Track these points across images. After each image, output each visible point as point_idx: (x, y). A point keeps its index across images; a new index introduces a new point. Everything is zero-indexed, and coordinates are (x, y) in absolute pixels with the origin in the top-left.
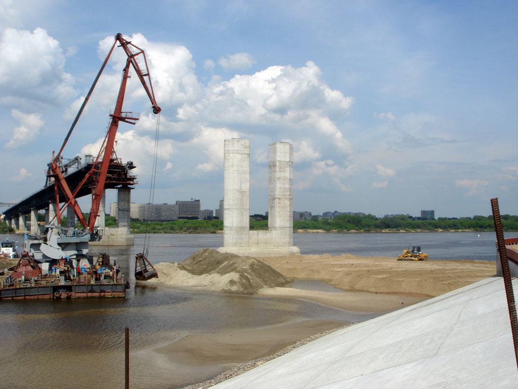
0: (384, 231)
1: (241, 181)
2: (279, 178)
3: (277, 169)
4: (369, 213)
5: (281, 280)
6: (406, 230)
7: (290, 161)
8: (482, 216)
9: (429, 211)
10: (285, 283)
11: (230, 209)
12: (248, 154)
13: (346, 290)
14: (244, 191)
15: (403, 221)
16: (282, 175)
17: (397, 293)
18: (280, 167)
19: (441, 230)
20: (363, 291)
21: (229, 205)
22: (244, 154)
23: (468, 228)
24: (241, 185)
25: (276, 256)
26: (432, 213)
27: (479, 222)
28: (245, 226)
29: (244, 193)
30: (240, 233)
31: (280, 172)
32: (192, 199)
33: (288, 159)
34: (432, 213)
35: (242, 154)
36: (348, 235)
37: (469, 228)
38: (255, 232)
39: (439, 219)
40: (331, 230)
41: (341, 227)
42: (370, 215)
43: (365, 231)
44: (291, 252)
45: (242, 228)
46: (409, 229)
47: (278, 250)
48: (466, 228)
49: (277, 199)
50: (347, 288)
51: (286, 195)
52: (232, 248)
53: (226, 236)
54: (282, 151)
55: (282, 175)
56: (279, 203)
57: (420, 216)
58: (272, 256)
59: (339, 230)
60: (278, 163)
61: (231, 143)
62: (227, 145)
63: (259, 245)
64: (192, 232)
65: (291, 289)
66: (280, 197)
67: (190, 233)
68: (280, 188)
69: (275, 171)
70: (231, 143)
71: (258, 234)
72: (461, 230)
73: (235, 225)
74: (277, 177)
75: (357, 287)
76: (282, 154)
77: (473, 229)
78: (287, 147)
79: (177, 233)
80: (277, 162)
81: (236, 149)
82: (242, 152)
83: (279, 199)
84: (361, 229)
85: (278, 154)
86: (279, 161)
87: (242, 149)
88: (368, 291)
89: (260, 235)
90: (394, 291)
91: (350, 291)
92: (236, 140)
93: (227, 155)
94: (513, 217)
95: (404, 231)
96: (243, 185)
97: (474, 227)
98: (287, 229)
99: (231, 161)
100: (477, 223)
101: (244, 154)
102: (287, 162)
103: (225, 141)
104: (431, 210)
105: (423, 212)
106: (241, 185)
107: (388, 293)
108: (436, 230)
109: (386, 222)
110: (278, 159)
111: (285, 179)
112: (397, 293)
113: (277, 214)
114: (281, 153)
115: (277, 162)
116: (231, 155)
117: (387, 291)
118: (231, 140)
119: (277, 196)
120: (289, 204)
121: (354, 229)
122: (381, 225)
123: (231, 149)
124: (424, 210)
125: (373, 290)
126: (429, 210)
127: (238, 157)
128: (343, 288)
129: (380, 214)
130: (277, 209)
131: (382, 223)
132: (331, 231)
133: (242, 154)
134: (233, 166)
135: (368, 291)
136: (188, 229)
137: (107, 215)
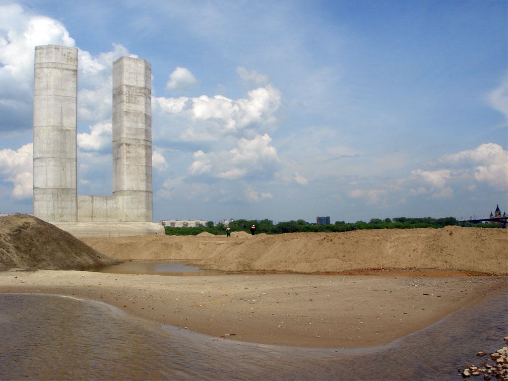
2: (127, 113)
3: (125, 98)
4: (266, 218)
5: (86, 259)
7: (145, 88)
8: (378, 220)
9: (324, 218)
10: (99, 266)
12: (74, 70)
13: (230, 273)
15: (300, 225)
16: (133, 107)
17: (375, 271)
18: (130, 96)
20: (274, 272)
22: (67, 69)
25: (122, 235)
26: (328, 219)
28: (69, 186)
29: (67, 133)
30: (59, 198)
33: (142, 84)
34: (328, 219)
35: (63, 69)
39: (337, 223)
42: (267, 220)
44: (148, 230)
49: (125, 146)
50: (233, 267)
51: (139, 140)
54: (132, 71)
55: (133, 107)
56: (128, 152)
57: (316, 223)
58: (116, 235)
60: (125, 89)
61: (45, 51)
66: (128, 142)
68: (129, 129)
69: (122, 102)
73: (51, 184)
74: (125, 110)
75: (258, 265)
76: (132, 76)
80: (125, 87)
81: (53, 61)
82: (64, 66)
83: (128, 145)
85: (126, 75)
86: (127, 86)
87: (63, 62)
88: (290, 272)
90: (363, 266)
91: (240, 273)
93: (38, 71)
94: (409, 219)
98: (142, 193)
101: (67, 69)
102: (141, 89)
103: (36, 49)
104: (326, 216)
105: (319, 219)
106: (62, 118)
107: (350, 273)
109: (283, 226)
110: (125, 82)
111: (137, 114)
112: (375, 271)
113: (124, 169)
114: (130, 73)
115: (125, 87)
116: (45, 70)
117: (346, 266)
119: (124, 141)
122: (278, 230)
123: (44, 60)
124: (320, 217)
125: (304, 267)
126: (324, 216)
127: (57, 73)
128: (224, 268)
130: (125, 162)
131: (279, 227)
134: (47, 88)
135: (290, 272)
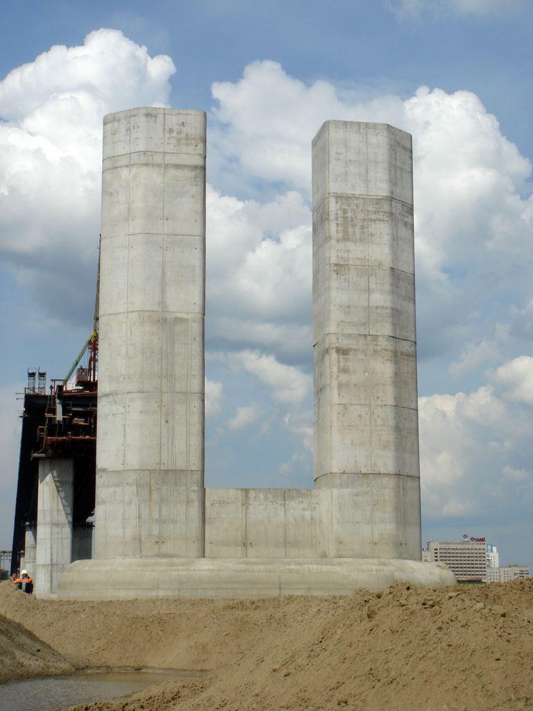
1: (163, 274)
22: (177, 166)
24: (163, 292)
28: (180, 464)
29: (179, 329)
30: (155, 496)
31: (346, 238)
32: (465, 536)
49: (334, 354)
51: (375, 337)
54: (352, 157)
68: (347, 308)
76: (352, 169)
80: (332, 201)
82: (170, 159)
101: (177, 166)
106: (163, 292)
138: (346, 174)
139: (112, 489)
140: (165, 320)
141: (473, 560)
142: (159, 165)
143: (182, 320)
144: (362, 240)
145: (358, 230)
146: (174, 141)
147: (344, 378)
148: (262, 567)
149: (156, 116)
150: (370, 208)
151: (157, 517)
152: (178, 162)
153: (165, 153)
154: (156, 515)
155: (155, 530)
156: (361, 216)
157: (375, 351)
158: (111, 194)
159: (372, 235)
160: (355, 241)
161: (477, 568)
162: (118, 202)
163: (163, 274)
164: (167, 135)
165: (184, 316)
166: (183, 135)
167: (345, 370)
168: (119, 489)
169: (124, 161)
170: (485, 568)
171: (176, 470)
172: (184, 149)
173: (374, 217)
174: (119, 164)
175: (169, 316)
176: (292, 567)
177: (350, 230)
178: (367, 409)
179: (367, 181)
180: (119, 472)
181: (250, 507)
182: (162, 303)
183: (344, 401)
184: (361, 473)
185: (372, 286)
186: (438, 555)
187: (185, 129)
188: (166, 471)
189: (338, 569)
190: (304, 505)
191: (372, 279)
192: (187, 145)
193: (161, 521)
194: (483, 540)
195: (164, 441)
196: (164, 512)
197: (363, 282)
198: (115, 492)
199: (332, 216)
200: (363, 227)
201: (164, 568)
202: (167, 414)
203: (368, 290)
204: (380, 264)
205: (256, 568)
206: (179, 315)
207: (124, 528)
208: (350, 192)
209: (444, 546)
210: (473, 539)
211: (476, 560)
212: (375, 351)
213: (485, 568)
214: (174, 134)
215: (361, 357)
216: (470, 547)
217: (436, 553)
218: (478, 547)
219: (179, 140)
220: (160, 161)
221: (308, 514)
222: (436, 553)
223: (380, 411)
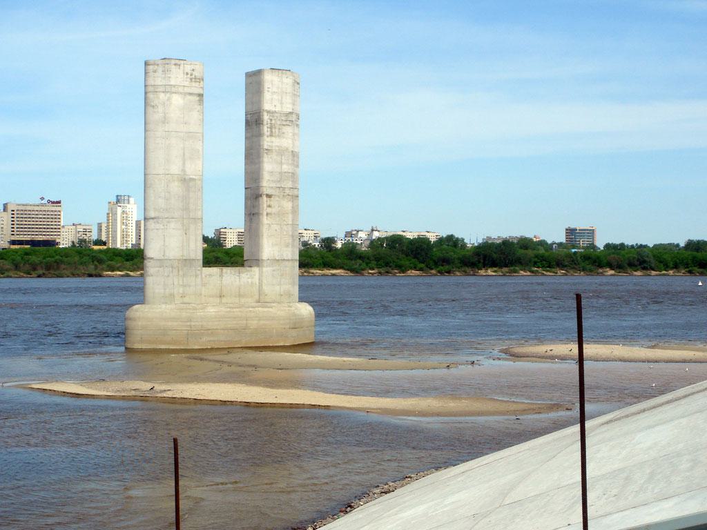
0: (482, 272)
1: (184, 154)
3: (266, 130)
6: (532, 272)
11: (158, 218)
14: (191, 179)
19: (612, 272)
21: (155, 209)
22: (190, 94)
23: (672, 269)
24: (184, 164)
27: (699, 255)
28: (193, 256)
29: (191, 184)
30: (181, 273)
31: (271, 135)
32: (42, 199)
34: (591, 233)
35: (186, 94)
36: (511, 278)
37: (676, 267)
38: (214, 270)
39: (608, 246)
40: (363, 270)
41: (387, 264)
43: (439, 272)
45: (187, 262)
46: (540, 270)
47: (265, 309)
48: (667, 268)
49: (265, 197)
51: (284, 188)
52: (164, 306)
53: (150, 281)
54: (275, 90)
59: (382, 270)
60: (266, 117)
62: (151, 74)
63: (224, 300)
64: (44, 274)
65: (388, 400)
66: (269, 192)
67: (39, 276)
68: (271, 173)
70: (160, 69)
71: (221, 276)
72: (657, 273)
76: (275, 97)
77: (683, 271)
78: (288, 81)
79: (8, 277)
80: (265, 114)
82: (187, 90)
83: (269, 196)
84: (432, 269)
86: (268, 112)
87: (187, 84)
89: (228, 277)
92: (173, 62)
95: (529, 273)
96: (188, 165)
97: (687, 265)
99: (160, 109)
100: (694, 258)
101: (190, 94)
103: (146, 64)
106: (184, 164)
108: (601, 270)
116: (162, 96)
118: (160, 62)
120: (290, 208)
121: (415, 268)
123: (159, 82)
124: (572, 227)
129: (473, 237)
132: (365, 273)
133: (186, 94)
136: (35, 269)
137: (268, 172)
138: (272, 99)
139: (157, 269)
140: (185, 179)
141: (48, 221)
142: (181, 93)
143: (193, 180)
144: (279, 136)
145: (277, 130)
146: (189, 80)
147: (269, 210)
148: (237, 310)
149: (179, 65)
150: (283, 118)
151: (181, 283)
152: (191, 91)
153: (184, 86)
154: (181, 283)
155: (181, 290)
156: (279, 123)
157: (283, 196)
158: (153, 106)
159: (283, 133)
160: (275, 137)
161: (52, 228)
162: (158, 112)
163: (184, 154)
164: (185, 76)
165: (194, 177)
166: (193, 76)
167: (269, 206)
168: (160, 269)
169: (161, 89)
170: (59, 229)
171: (190, 260)
172: (194, 84)
173: (284, 123)
174: (158, 90)
175: (187, 177)
176: (251, 309)
177: (273, 130)
178: (279, 226)
179: (282, 103)
180: (161, 260)
181: (224, 278)
182: (183, 170)
183: (268, 222)
184: (276, 259)
185: (283, 161)
186: (15, 216)
187: (194, 73)
188: (185, 260)
189: (270, 309)
190: (248, 276)
191: (283, 157)
192: (195, 82)
193: (184, 286)
194: (59, 202)
195: (185, 244)
196: (185, 281)
197: (279, 159)
198: (159, 271)
199: (265, 123)
200: (279, 129)
201: (191, 311)
202: (186, 230)
203: (281, 163)
204: (287, 149)
205: (235, 310)
206: (191, 177)
207: (165, 289)
208: (274, 109)
209: (20, 208)
210: (49, 201)
211: (52, 222)
212: (283, 196)
213: (59, 229)
214: (189, 76)
215: (277, 199)
216: (46, 208)
217: (13, 214)
218: (54, 209)
219: (191, 79)
220: (182, 91)
221: (250, 280)
222: (13, 214)
223: (285, 227)
